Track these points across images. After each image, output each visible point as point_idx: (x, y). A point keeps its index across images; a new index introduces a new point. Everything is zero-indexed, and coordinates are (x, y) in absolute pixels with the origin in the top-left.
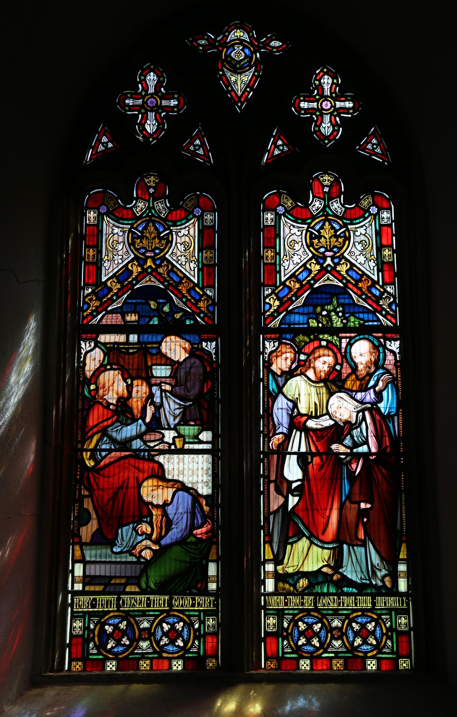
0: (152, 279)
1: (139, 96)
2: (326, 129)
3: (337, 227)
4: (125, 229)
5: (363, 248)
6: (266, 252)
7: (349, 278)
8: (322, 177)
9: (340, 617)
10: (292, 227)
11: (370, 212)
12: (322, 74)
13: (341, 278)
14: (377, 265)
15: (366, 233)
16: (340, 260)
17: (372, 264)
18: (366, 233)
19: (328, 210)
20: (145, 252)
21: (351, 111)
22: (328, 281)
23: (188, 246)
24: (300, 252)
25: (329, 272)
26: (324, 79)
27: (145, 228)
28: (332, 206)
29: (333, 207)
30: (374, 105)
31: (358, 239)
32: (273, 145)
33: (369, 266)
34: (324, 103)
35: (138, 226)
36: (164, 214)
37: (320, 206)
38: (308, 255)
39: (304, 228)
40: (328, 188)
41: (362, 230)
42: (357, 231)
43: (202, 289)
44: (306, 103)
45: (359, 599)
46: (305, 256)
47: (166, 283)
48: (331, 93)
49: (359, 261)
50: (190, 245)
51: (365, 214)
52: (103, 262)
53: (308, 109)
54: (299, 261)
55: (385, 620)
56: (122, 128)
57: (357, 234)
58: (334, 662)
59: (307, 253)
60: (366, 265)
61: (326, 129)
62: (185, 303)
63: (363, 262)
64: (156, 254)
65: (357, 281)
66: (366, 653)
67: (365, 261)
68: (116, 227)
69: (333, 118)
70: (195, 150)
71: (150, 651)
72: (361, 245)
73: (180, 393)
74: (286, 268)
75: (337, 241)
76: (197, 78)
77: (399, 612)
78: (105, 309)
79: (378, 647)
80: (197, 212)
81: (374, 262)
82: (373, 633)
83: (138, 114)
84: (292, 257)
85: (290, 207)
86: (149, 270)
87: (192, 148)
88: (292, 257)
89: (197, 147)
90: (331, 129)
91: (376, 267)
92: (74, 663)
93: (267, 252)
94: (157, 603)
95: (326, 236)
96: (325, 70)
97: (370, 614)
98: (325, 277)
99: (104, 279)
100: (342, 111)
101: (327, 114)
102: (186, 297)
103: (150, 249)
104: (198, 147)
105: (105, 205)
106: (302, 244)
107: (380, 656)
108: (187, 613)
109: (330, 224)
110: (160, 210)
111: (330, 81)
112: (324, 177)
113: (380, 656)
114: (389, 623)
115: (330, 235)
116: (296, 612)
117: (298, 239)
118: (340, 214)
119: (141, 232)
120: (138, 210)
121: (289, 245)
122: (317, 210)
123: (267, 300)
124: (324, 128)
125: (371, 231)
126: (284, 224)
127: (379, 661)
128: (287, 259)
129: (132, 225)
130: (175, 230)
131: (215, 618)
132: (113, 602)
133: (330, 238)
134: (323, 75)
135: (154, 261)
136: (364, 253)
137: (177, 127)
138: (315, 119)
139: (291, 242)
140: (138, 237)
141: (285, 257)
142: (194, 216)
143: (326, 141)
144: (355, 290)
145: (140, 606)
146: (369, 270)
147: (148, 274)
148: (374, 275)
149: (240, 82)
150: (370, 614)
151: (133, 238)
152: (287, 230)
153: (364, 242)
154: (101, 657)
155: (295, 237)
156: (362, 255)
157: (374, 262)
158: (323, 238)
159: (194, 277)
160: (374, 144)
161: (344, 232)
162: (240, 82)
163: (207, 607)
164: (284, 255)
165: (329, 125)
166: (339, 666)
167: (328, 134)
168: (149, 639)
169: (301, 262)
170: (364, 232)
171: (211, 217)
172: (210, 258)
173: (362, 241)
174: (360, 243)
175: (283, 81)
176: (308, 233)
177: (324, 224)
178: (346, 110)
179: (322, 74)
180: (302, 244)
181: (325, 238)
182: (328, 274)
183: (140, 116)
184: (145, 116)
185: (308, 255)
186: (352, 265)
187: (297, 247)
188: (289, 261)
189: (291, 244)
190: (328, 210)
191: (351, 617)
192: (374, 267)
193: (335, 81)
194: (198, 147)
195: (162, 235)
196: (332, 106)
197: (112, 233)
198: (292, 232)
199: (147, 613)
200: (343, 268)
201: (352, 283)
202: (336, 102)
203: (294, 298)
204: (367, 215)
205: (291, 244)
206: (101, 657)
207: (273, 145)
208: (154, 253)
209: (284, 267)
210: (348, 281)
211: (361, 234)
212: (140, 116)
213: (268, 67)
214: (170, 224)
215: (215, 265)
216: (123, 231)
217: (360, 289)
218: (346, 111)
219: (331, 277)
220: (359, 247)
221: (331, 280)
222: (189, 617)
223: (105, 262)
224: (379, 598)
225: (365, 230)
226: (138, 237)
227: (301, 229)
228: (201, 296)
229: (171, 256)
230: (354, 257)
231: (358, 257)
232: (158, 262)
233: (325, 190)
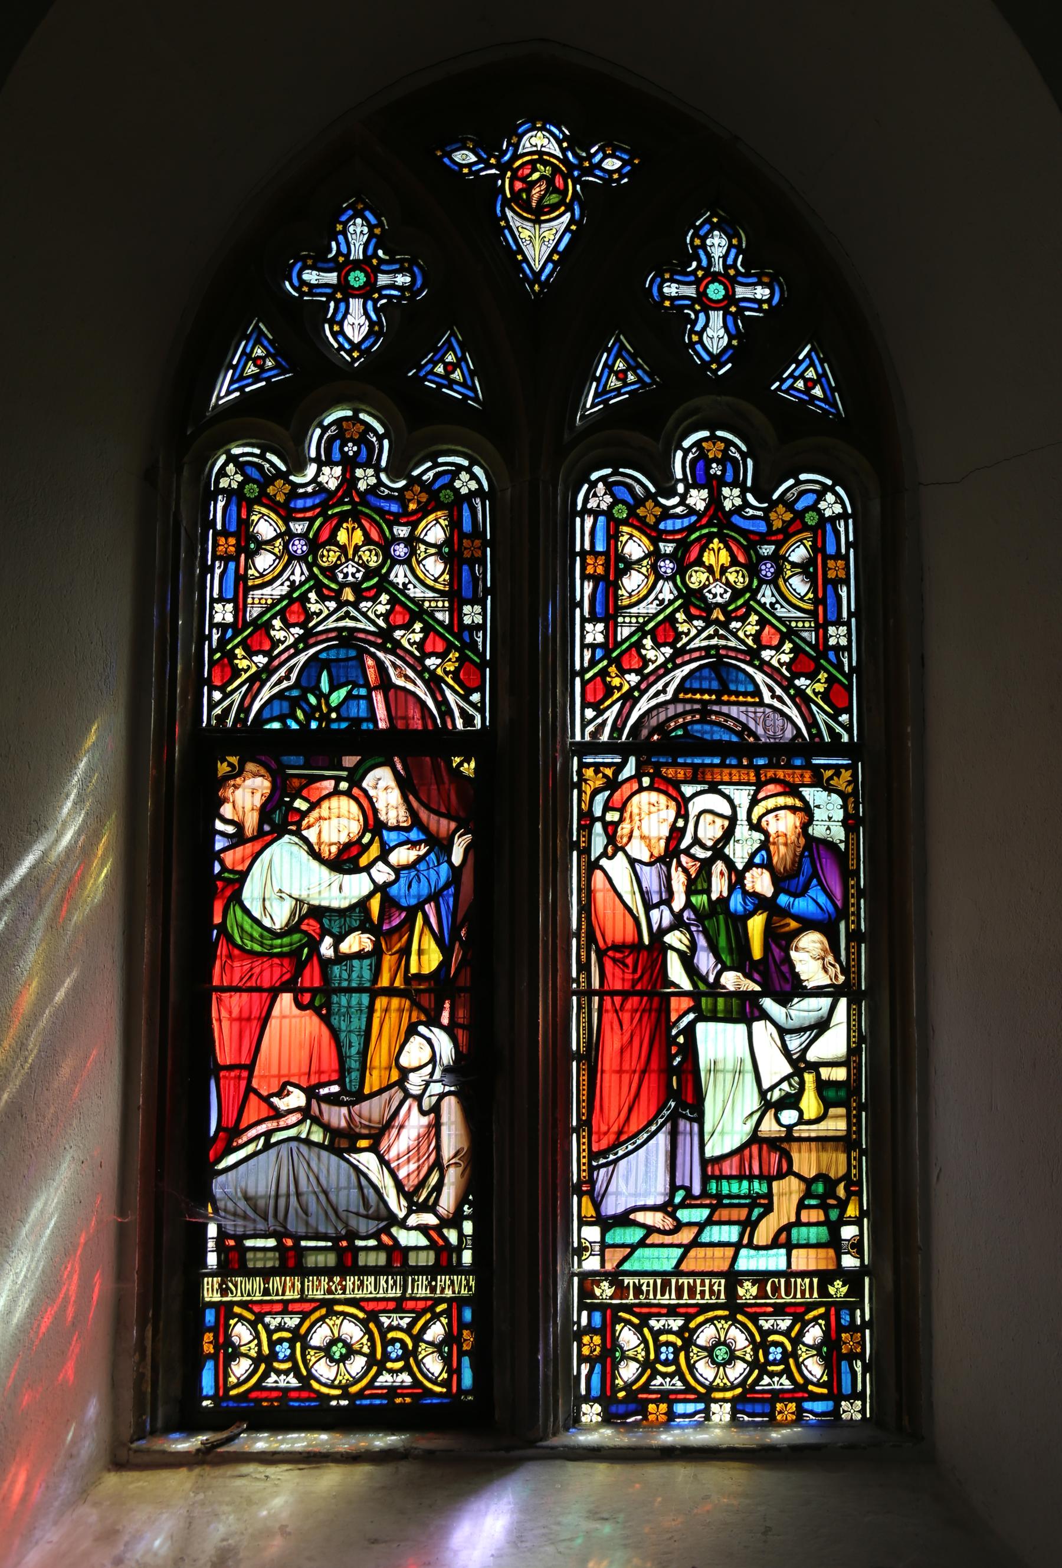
1: (331, 265)
2: (715, 340)
12: (707, 227)
26: (712, 237)
30: (815, 302)
32: (607, 370)
48: (726, 267)
56: (300, 324)
61: (715, 340)
69: (730, 319)
73: (736, 911)
76: (450, 233)
83: (328, 302)
96: (715, 220)
111: (724, 242)
134: (710, 231)
137: (406, 330)
149: (539, 242)
162: (539, 242)
175: (626, 239)
179: (707, 227)
183: (332, 304)
184: (342, 306)
193: (735, 242)
207: (607, 370)
212: (332, 304)
213: (599, 207)
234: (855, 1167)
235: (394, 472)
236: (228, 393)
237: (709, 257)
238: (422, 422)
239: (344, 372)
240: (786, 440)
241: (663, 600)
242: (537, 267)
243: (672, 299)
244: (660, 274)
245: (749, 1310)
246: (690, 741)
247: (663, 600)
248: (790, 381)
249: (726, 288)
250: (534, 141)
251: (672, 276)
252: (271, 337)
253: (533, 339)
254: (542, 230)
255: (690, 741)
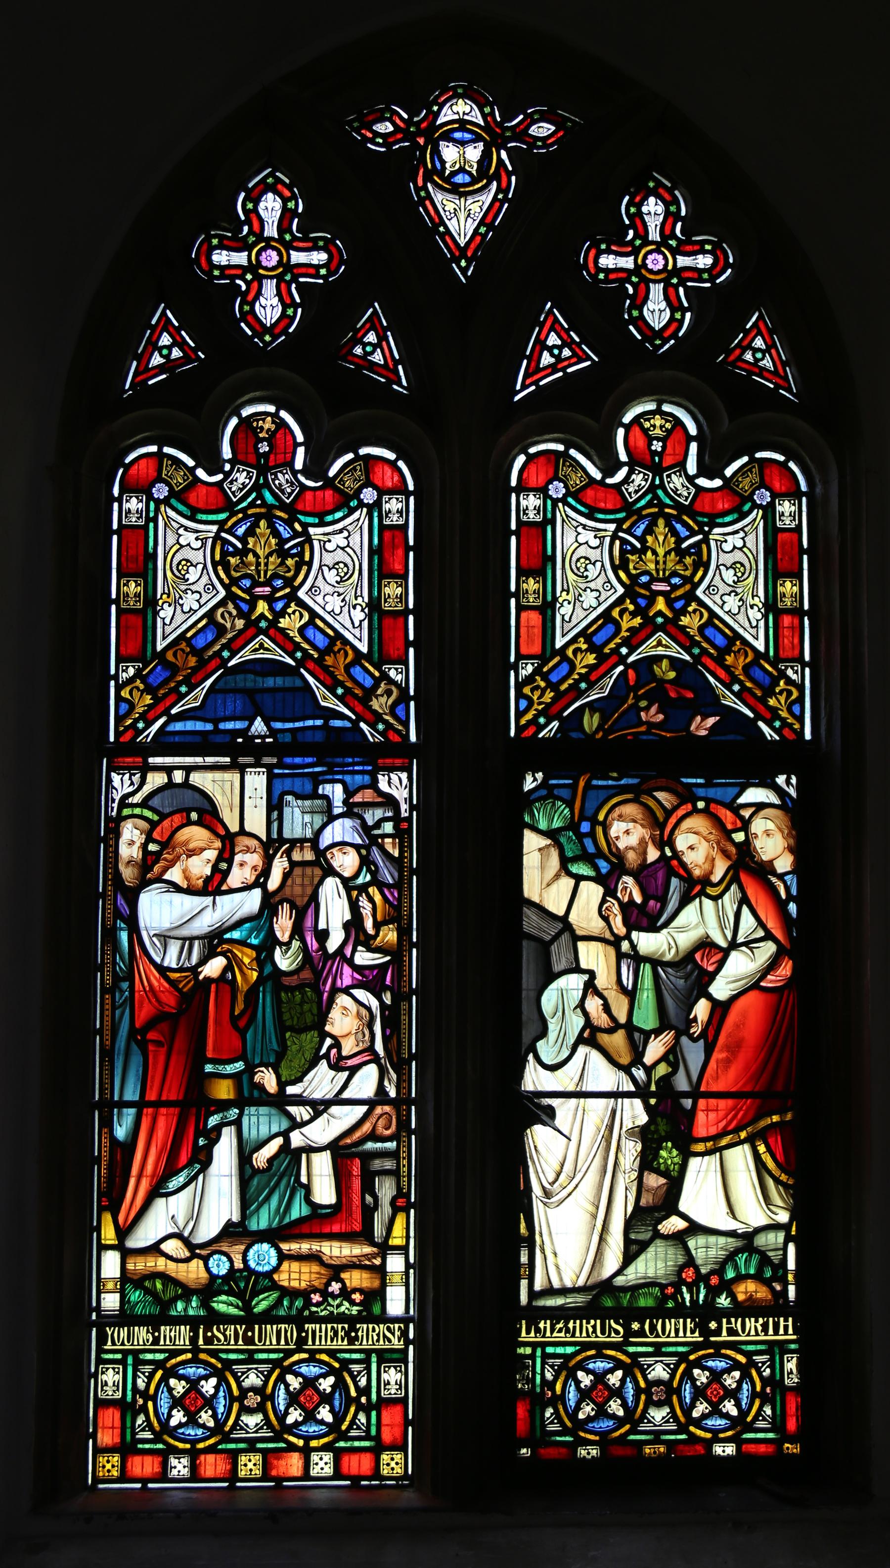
0: (664, 642)
3: (684, 532)
4: (603, 534)
5: (338, 579)
6: (124, 585)
7: (704, 645)
8: (649, 420)
9: (667, 1360)
10: (580, 529)
11: (754, 501)
13: (290, 647)
14: (370, 616)
15: (744, 546)
16: (287, 606)
17: (358, 615)
18: (348, 546)
19: (660, 492)
20: (253, 586)
21: (323, 272)
22: (660, 648)
23: (346, 574)
24: (598, 584)
25: (265, 632)
27: (649, 531)
28: (669, 482)
29: (671, 485)
31: (329, 559)
33: (748, 618)
34: (649, 257)
35: (235, 524)
36: (687, 498)
37: (643, 483)
38: (218, 592)
39: (605, 530)
40: (660, 444)
41: (340, 540)
42: (726, 541)
43: (774, 665)
44: (225, 252)
45: (286, 1331)
46: (210, 596)
47: (299, 655)
49: (726, 608)
50: (351, 568)
51: (744, 504)
52: (558, 605)
53: (229, 267)
54: (195, 606)
55: (239, 1374)
56: (213, 307)
57: (727, 547)
58: (243, 1459)
59: (612, 586)
60: (344, 619)
61: (269, 310)
62: (341, 699)
63: (337, 611)
64: (275, 590)
65: (323, 653)
66: (715, 1432)
67: (739, 607)
68: (186, 529)
70: (367, 354)
71: (673, 1427)
72: (334, 572)
74: (167, 621)
75: (282, 563)
77: (386, 1357)
78: (166, 712)
79: (740, 1423)
80: (369, 495)
81: (363, 610)
82: (618, 1392)
84: (580, 595)
85: (181, 484)
86: (660, 620)
87: (748, 356)
88: (181, 597)
89: (369, 349)
90: (667, 315)
91: (366, 621)
92: (102, 1460)
93: (126, 585)
94: (320, 1337)
95: (258, 550)
97: (729, 1352)
98: (652, 641)
99: (559, 643)
100: (303, 270)
101: (271, 277)
102: (741, 683)
103: (262, 580)
104: (376, 348)
105: (560, 481)
106: (603, 566)
107: (342, 1444)
108: (223, 1356)
109: (668, 524)
110: (677, 490)
112: (652, 421)
113: (342, 1444)
114: (768, 1370)
115: (267, 551)
116: (570, 1350)
117: (594, 555)
118: (686, 501)
119: (243, 539)
120: (233, 489)
121: (574, 567)
122: (636, 492)
123: (125, 693)
124: (652, 312)
125: (756, 542)
126: (166, 523)
127: (338, 1455)
128: (569, 598)
129: (221, 524)
130: (321, 537)
131: (385, 1367)
132: (318, 1334)
133: (267, 557)
135: (669, 603)
136: (739, 590)
138: (244, 288)
139: (179, 563)
140: (237, 552)
141: (564, 593)
142: (755, 506)
143: (658, 342)
144: (318, 670)
145: (335, 1343)
146: (747, 625)
147: (658, 628)
148: (360, 640)
150: (729, 1352)
151: (623, 552)
152: (171, 540)
153: (342, 565)
154: (160, 1446)
155: (186, 553)
156: (733, 594)
157: (363, 610)
158: (649, 554)
159: (164, 638)
160: (759, 350)
161: (697, 545)
163: (588, 1336)
164: (563, 590)
165: (663, 305)
166: (253, 1468)
167: (661, 325)
168: (668, 1402)
169: (201, 607)
170: (343, 543)
171: (793, 508)
172: (135, 596)
173: (337, 563)
174: (333, 567)
175: (558, 212)
176: (617, 542)
177: (256, 525)
178: (312, 269)
180: (603, 566)
181: (256, 555)
182: (262, 636)
185: (218, 592)
186: (313, 614)
187: (592, 572)
188: (172, 607)
189: (579, 565)
190: (660, 492)
191: (168, 1365)
192: (757, 621)
194: (376, 348)
195: (287, 546)
196: (280, 262)
197: (178, 543)
198: (581, 539)
199: (663, 1349)
200: (291, 623)
201: (710, 655)
202: (291, 252)
203: (736, 688)
204: (747, 507)
205: (579, 565)
206: (160, 1446)
208: (272, 586)
209: (164, 619)
210: (704, 651)
211: (735, 547)
214: (310, 520)
215: (406, 612)
216: (600, 538)
217: (727, 669)
218: (312, 271)
219: (268, 643)
220: (332, 576)
221: (267, 649)
222: (748, 1355)
223: (562, 605)
224: (323, 1326)
225: (743, 539)
226: (634, 551)
227: (603, 534)
228: (377, 682)
229: (707, 592)
230: (717, 598)
231: (726, 598)
232: (679, 605)
233: (653, 448)
234: (404, 1166)
235: (704, 470)
236: (524, 387)
237: (261, 221)
238: (735, 418)
239: (264, 356)
240: (340, 407)
241: (188, 579)
242: (462, 242)
243: (607, 271)
244: (595, 245)
245: (743, 1347)
246: (651, 737)
247: (188, 579)
248: (738, 352)
249: (280, 254)
250: (455, 108)
251: (608, 247)
252: (537, 329)
253: (466, 319)
254: (468, 202)
255: (651, 737)
